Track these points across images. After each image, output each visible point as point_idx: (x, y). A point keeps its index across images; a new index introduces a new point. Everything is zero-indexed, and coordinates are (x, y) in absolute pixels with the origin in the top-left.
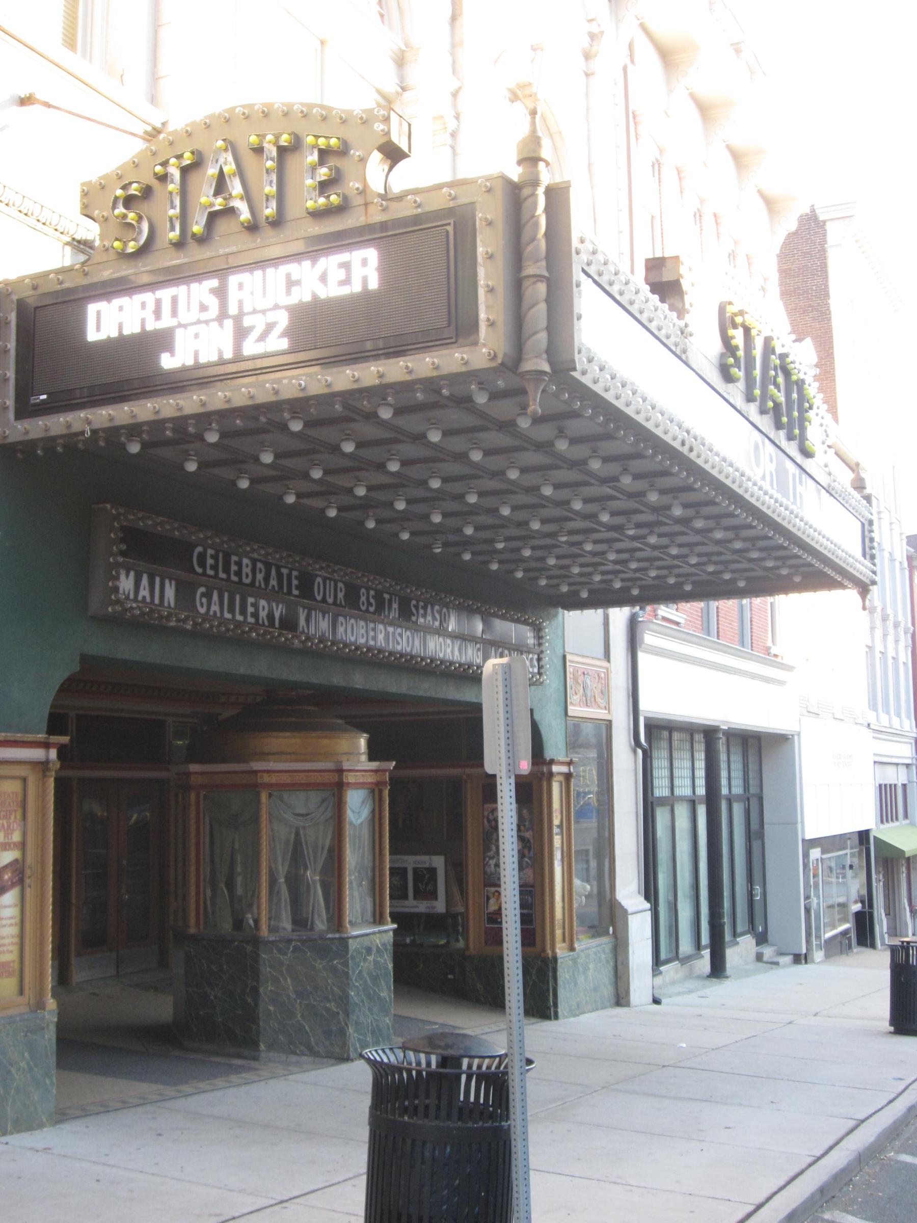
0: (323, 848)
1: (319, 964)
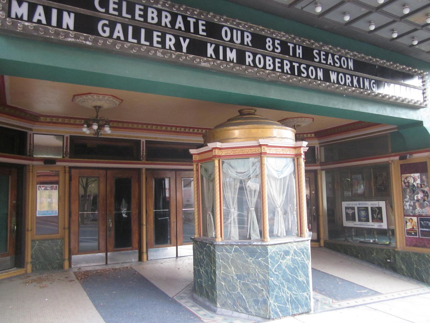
0: (255, 191)
1: (250, 260)
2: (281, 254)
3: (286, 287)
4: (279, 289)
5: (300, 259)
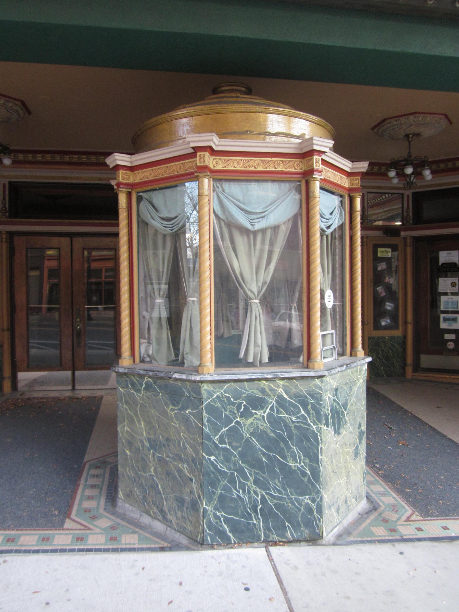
2: (240, 405)
3: (252, 479)
4: (232, 481)
5: (294, 419)
